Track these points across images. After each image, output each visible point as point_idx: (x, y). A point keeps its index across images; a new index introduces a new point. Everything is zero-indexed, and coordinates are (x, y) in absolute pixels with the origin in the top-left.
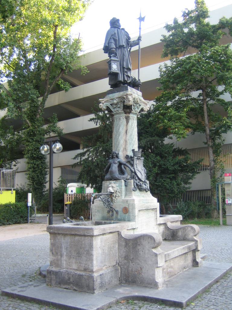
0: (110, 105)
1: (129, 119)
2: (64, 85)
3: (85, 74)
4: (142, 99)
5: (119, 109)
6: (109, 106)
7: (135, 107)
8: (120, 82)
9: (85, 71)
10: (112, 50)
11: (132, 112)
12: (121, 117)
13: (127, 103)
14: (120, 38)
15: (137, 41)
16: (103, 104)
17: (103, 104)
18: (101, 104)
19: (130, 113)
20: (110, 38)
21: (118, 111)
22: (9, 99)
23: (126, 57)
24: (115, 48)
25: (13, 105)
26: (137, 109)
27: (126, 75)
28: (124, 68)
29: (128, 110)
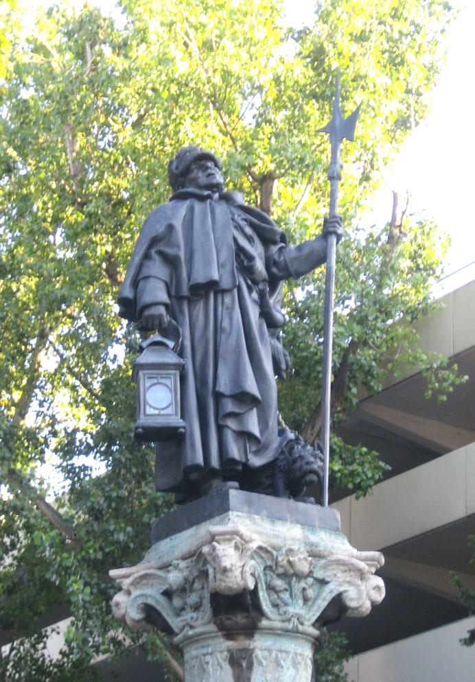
0: (162, 600)
1: (250, 666)
2: (345, 463)
3: (448, 394)
4: (355, 551)
5: (195, 615)
6: (157, 601)
7: (286, 596)
8: (207, 473)
9: (445, 380)
10: (147, 313)
11: (264, 623)
12: (208, 658)
13: (218, 583)
14: (197, 244)
15: (318, 246)
16: (129, 593)
17: (129, 593)
18: (119, 598)
19: (251, 630)
20: (147, 256)
21: (192, 627)
22: (69, 563)
23: (234, 335)
24: (166, 305)
25: (88, 590)
26: (296, 608)
27: (234, 431)
28: (218, 396)
29: (240, 619)
